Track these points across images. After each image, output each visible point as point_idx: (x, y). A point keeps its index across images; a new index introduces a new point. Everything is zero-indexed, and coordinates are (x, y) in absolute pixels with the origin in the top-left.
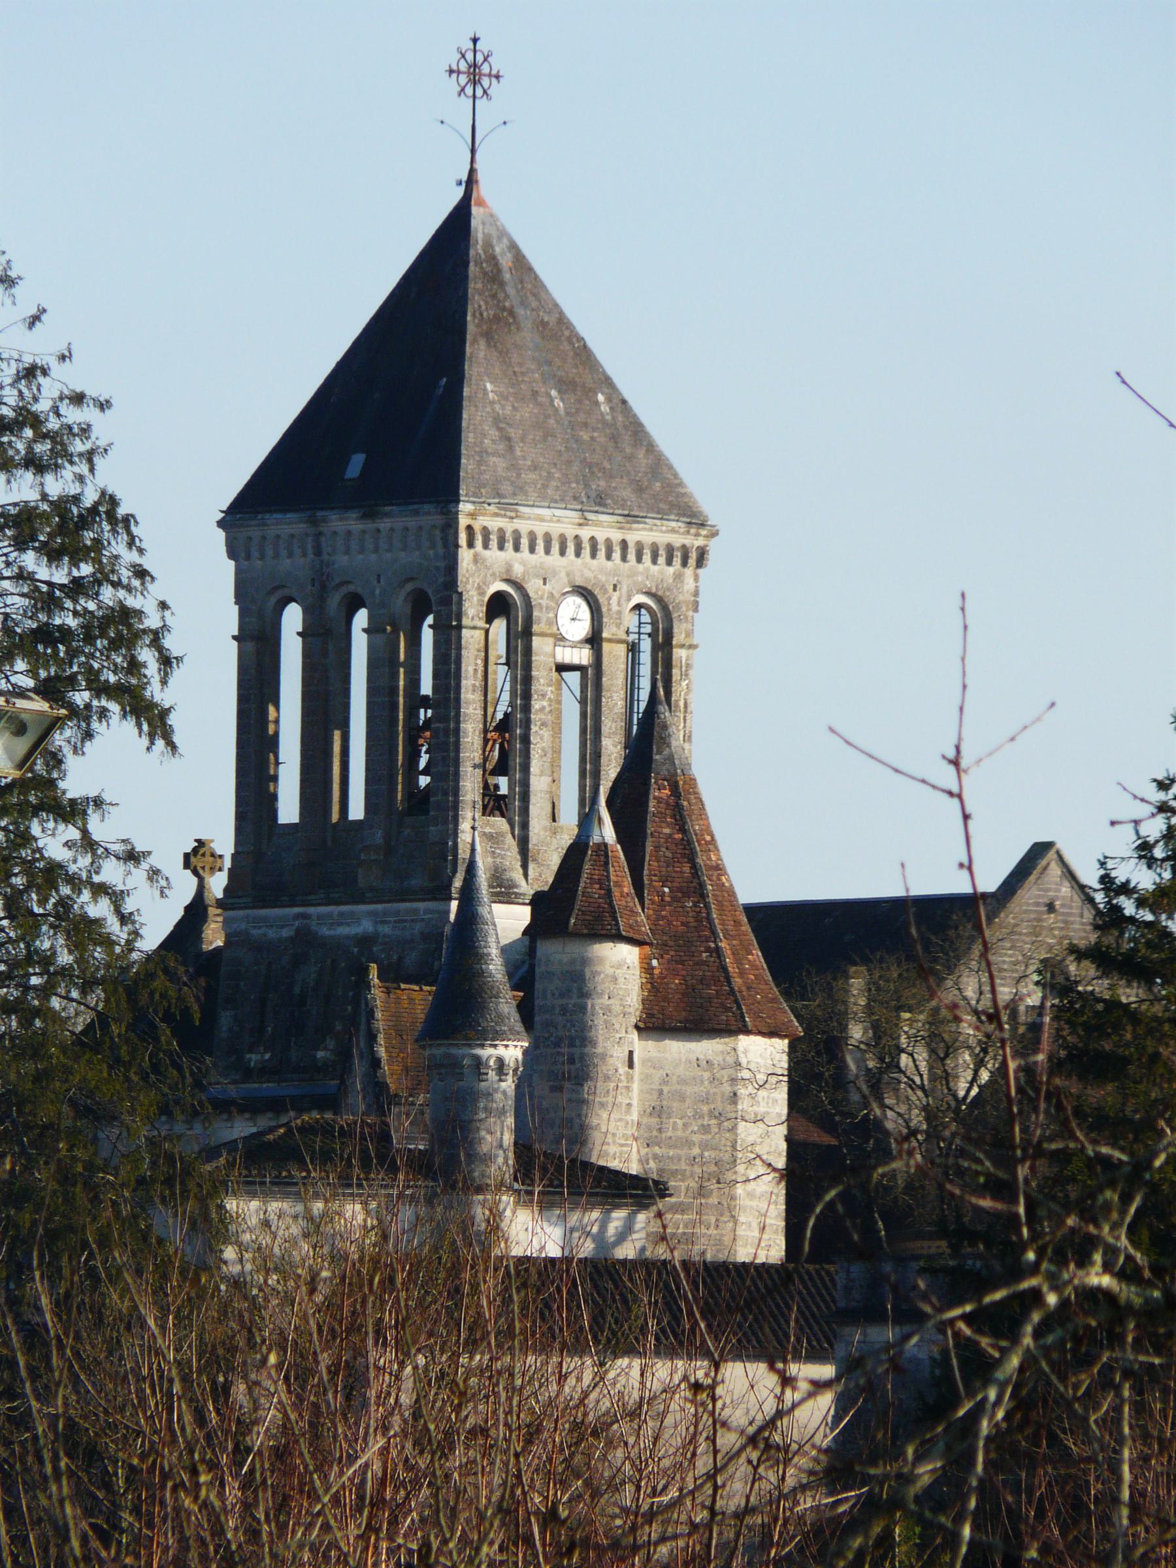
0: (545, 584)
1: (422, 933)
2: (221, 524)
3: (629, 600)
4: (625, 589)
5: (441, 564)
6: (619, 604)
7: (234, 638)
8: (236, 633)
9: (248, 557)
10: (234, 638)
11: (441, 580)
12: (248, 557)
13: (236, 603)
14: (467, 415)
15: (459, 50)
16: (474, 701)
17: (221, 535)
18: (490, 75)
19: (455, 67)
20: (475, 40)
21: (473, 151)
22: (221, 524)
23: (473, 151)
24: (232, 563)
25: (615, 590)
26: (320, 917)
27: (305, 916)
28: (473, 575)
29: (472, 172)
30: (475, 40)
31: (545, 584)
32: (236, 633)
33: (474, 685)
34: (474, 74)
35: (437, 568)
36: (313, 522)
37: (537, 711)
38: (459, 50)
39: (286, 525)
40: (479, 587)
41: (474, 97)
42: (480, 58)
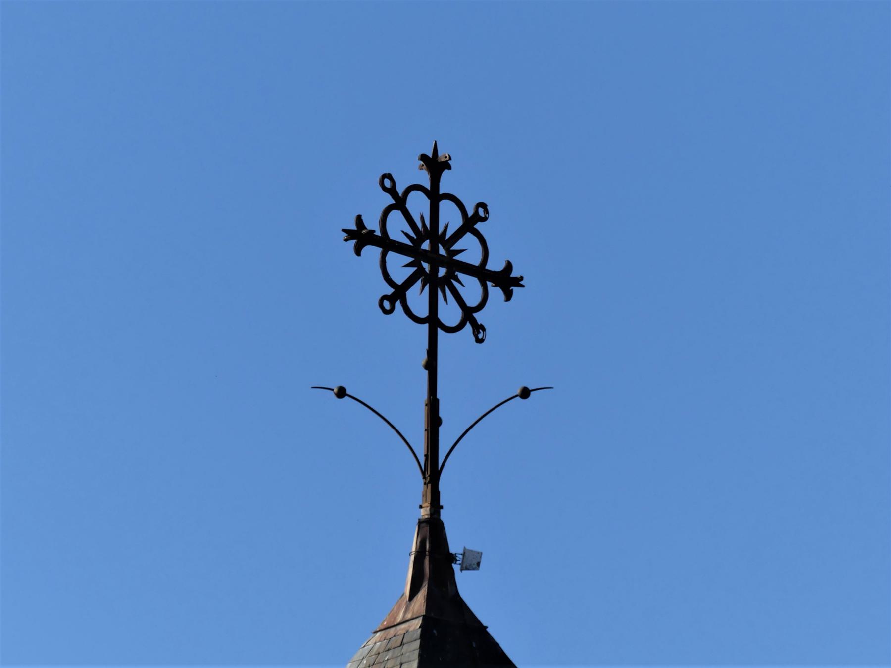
15: (387, 183)
21: (432, 471)
23: (432, 471)
34: (433, 256)
38: (387, 183)
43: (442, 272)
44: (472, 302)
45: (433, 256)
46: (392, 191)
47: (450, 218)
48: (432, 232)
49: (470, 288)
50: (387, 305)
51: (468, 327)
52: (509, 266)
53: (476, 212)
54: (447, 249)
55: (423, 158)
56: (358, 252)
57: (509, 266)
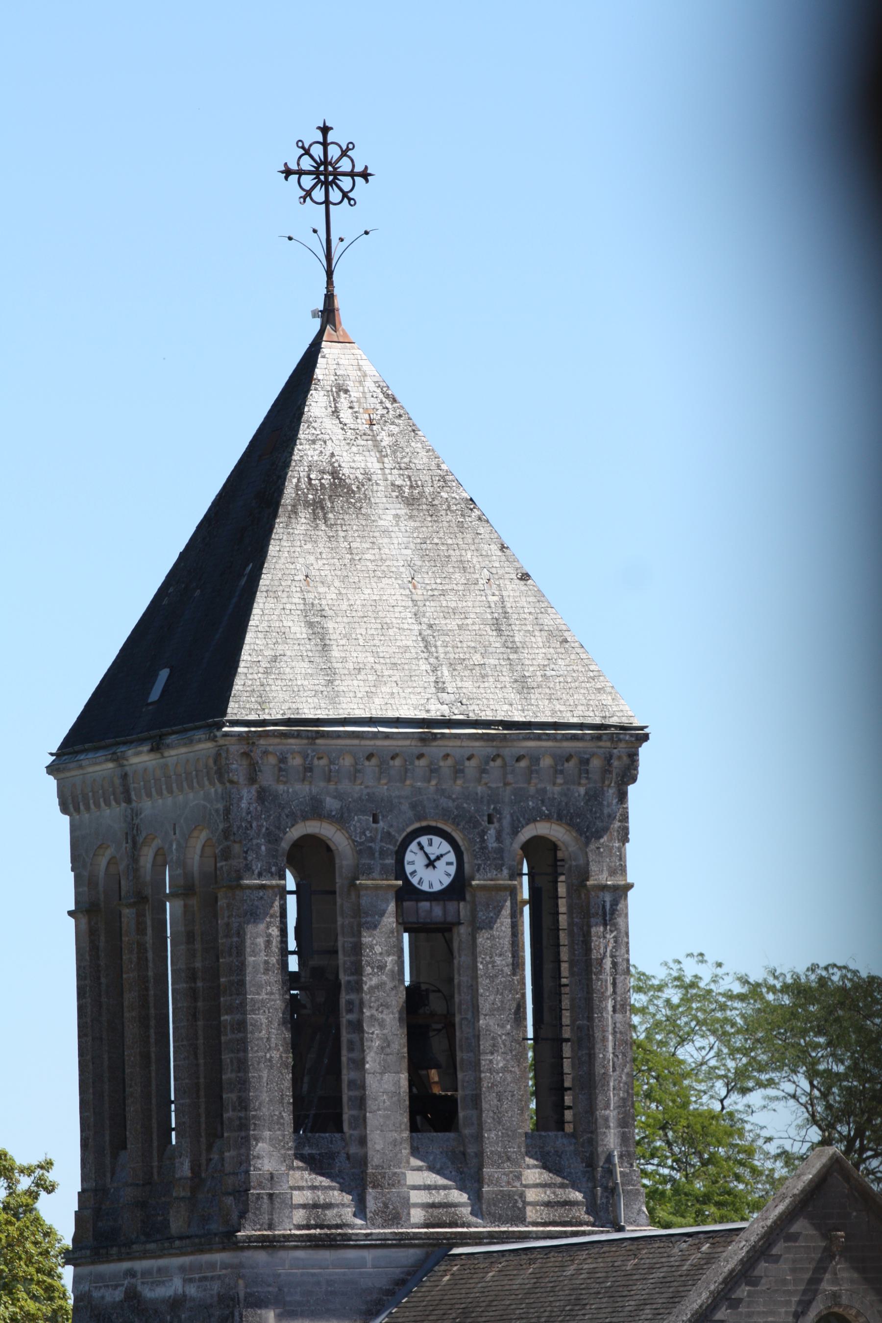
0: (375, 821)
1: (218, 1294)
2: (51, 769)
3: (515, 832)
4: (506, 822)
5: (220, 806)
6: (499, 838)
7: (70, 913)
8: (73, 908)
9: (77, 810)
10: (70, 913)
11: (221, 826)
12: (77, 810)
13: (72, 870)
14: (263, 613)
15: (300, 144)
16: (268, 983)
17: (51, 783)
18: (352, 174)
19: (293, 166)
20: (325, 130)
21: (330, 273)
22: (51, 769)
23: (330, 273)
24: (67, 818)
25: (490, 821)
26: (146, 1273)
27: (131, 1273)
28: (258, 818)
29: (329, 298)
30: (325, 130)
31: (375, 821)
32: (73, 908)
33: (266, 962)
34: (326, 173)
35: (217, 811)
36: (116, 759)
37: (372, 988)
38: (300, 144)
39: (98, 768)
40: (269, 833)
41: (327, 202)
42: (334, 152)
43: (322, 168)
44: (346, 189)
45: (326, 173)
46: (350, 199)
47: (319, 194)
48: (327, 184)
49: (346, 183)
50: (351, 146)
51: (346, 200)
52: (286, 178)
53: (348, 147)
54: (319, 179)
55: (319, 128)
56: (366, 168)
57: (286, 178)
